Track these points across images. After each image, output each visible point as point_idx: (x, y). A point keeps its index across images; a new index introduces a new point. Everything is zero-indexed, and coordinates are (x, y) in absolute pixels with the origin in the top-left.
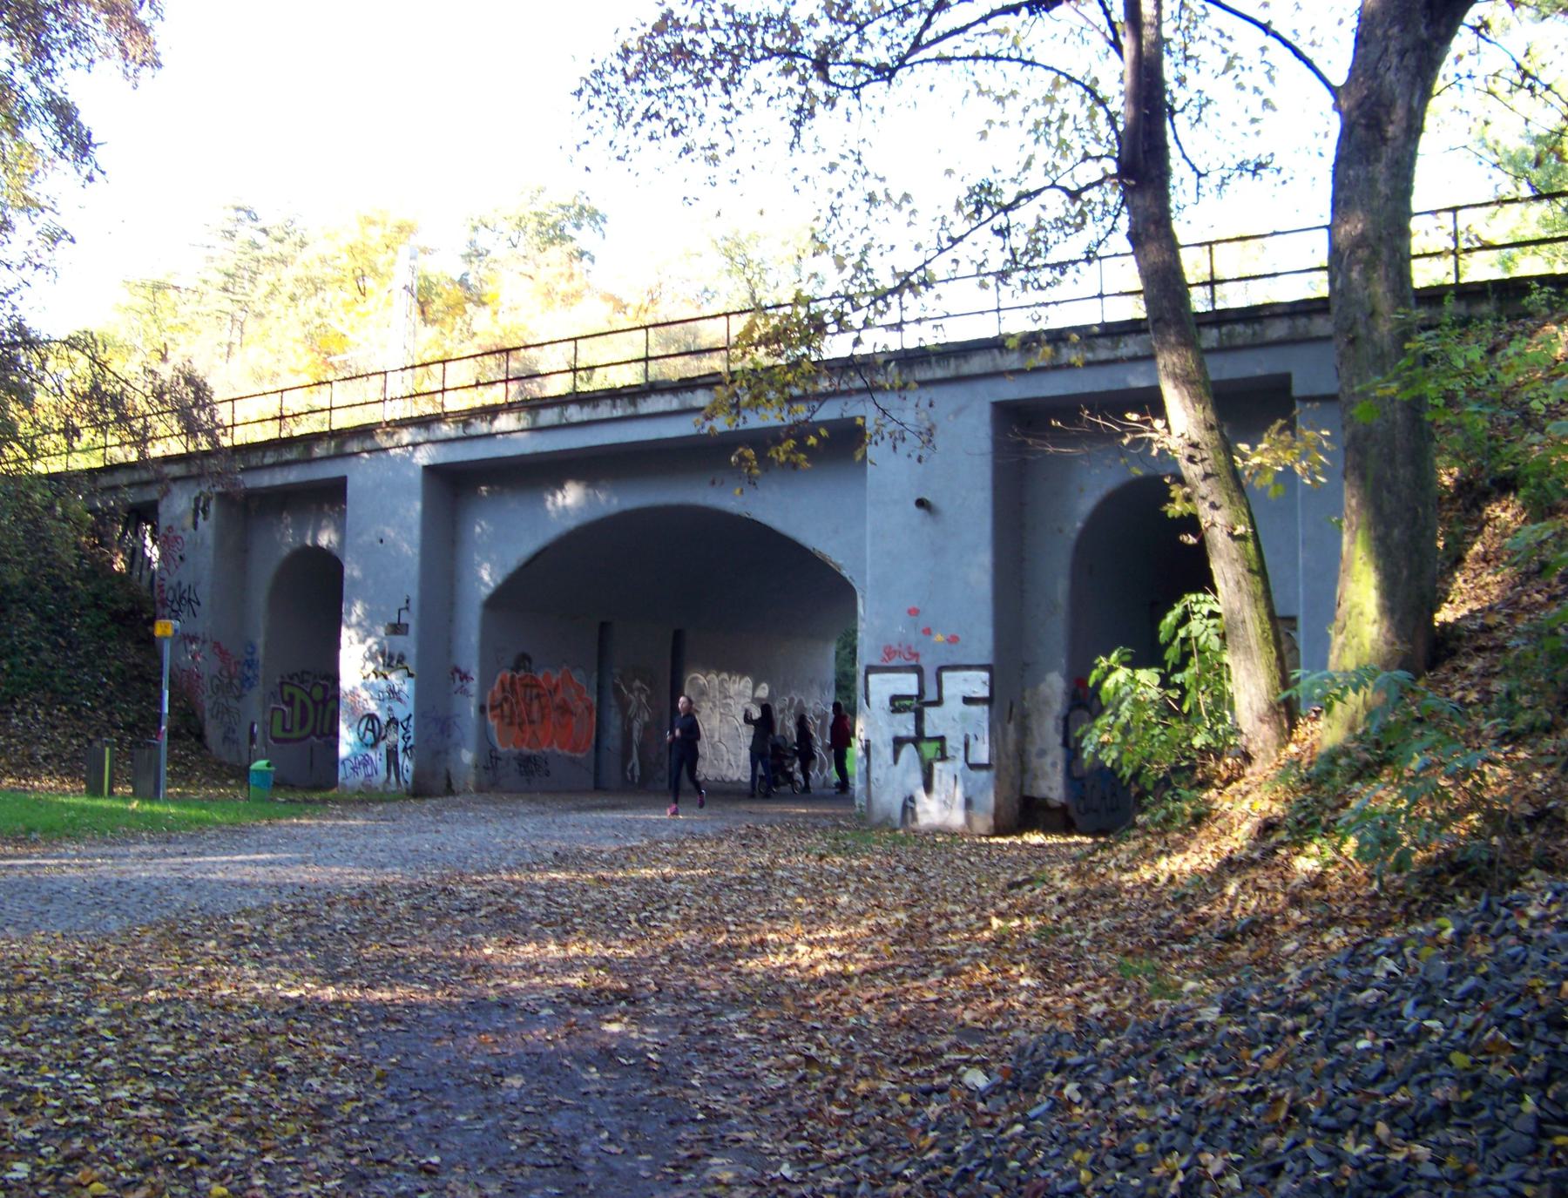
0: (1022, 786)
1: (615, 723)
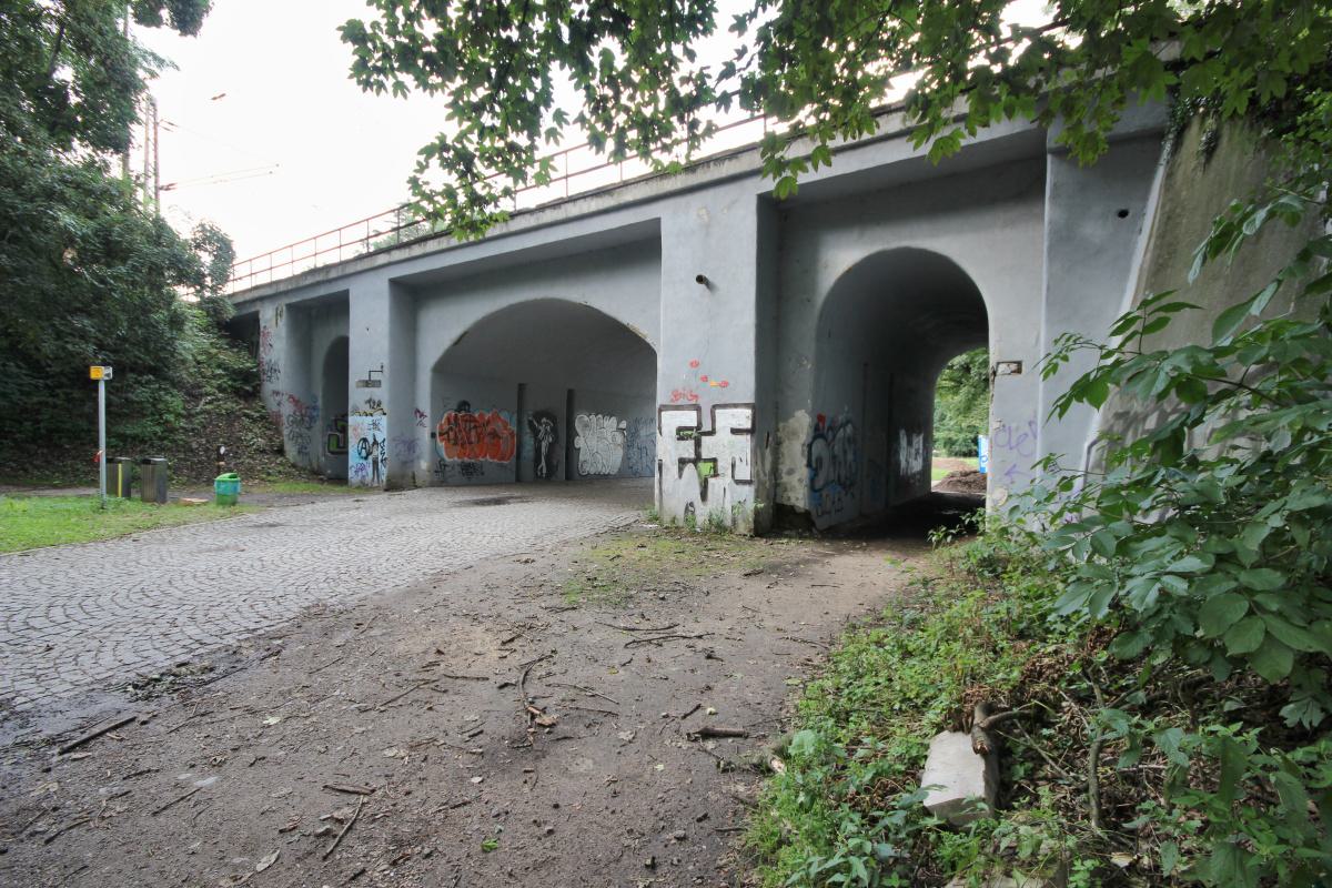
0: (775, 495)
1: (529, 441)
